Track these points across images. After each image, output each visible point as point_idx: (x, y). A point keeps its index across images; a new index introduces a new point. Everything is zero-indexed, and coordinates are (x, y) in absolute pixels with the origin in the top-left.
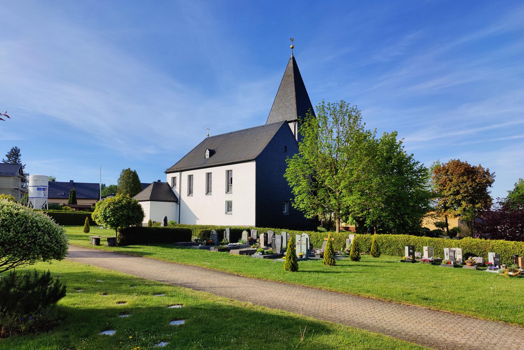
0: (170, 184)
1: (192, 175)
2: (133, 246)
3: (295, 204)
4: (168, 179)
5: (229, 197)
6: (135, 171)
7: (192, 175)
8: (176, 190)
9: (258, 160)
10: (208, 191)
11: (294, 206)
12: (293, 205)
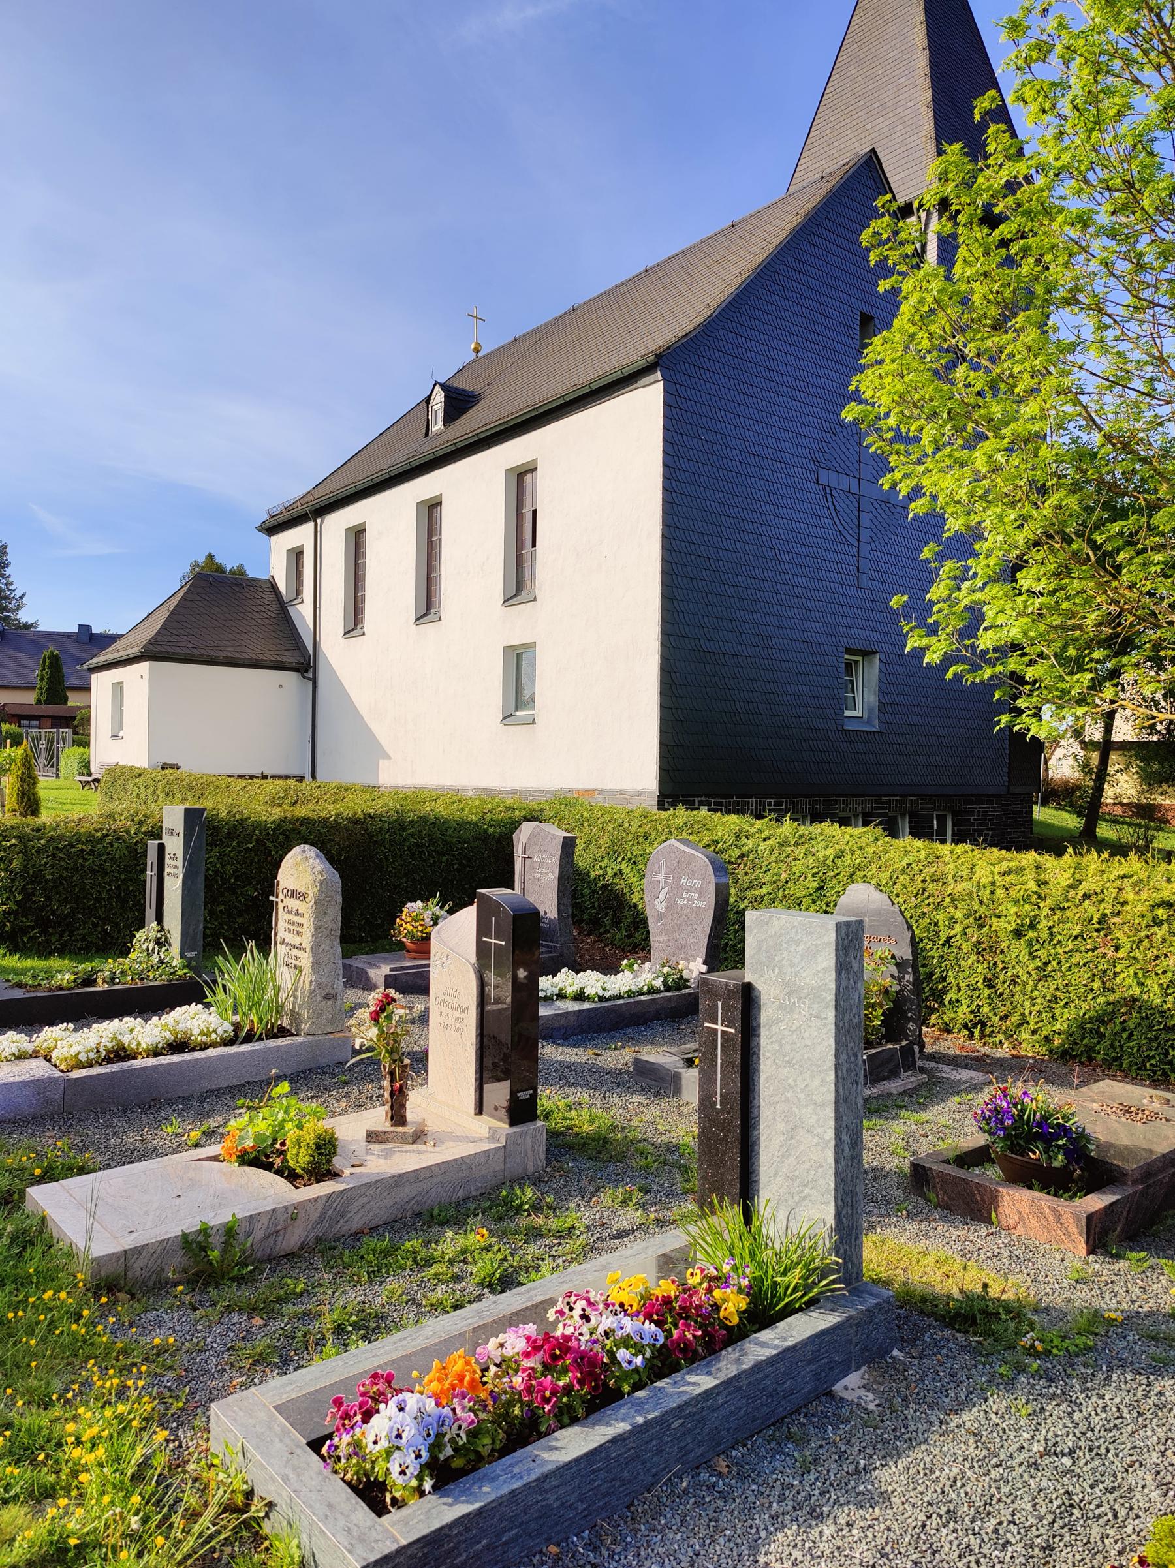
0: (282, 586)
1: (531, 646)
2: (150, 874)
3: (933, 630)
4: (272, 561)
5: (519, 625)
6: (241, 567)
7: (531, 646)
8: (303, 612)
9: (678, 365)
10: (428, 604)
11: (920, 652)
12: (914, 642)
